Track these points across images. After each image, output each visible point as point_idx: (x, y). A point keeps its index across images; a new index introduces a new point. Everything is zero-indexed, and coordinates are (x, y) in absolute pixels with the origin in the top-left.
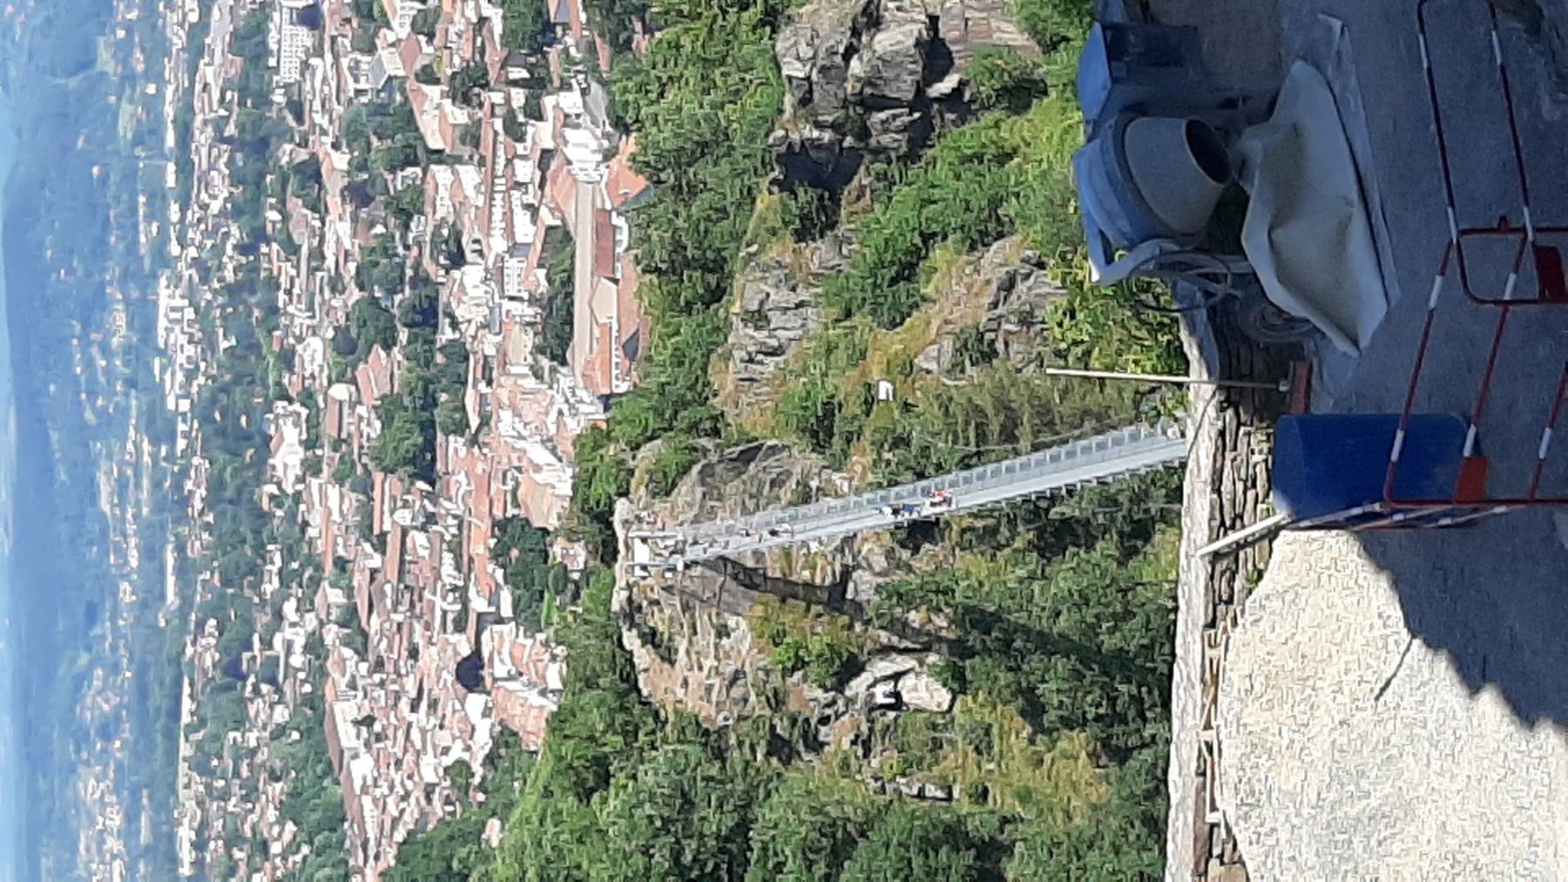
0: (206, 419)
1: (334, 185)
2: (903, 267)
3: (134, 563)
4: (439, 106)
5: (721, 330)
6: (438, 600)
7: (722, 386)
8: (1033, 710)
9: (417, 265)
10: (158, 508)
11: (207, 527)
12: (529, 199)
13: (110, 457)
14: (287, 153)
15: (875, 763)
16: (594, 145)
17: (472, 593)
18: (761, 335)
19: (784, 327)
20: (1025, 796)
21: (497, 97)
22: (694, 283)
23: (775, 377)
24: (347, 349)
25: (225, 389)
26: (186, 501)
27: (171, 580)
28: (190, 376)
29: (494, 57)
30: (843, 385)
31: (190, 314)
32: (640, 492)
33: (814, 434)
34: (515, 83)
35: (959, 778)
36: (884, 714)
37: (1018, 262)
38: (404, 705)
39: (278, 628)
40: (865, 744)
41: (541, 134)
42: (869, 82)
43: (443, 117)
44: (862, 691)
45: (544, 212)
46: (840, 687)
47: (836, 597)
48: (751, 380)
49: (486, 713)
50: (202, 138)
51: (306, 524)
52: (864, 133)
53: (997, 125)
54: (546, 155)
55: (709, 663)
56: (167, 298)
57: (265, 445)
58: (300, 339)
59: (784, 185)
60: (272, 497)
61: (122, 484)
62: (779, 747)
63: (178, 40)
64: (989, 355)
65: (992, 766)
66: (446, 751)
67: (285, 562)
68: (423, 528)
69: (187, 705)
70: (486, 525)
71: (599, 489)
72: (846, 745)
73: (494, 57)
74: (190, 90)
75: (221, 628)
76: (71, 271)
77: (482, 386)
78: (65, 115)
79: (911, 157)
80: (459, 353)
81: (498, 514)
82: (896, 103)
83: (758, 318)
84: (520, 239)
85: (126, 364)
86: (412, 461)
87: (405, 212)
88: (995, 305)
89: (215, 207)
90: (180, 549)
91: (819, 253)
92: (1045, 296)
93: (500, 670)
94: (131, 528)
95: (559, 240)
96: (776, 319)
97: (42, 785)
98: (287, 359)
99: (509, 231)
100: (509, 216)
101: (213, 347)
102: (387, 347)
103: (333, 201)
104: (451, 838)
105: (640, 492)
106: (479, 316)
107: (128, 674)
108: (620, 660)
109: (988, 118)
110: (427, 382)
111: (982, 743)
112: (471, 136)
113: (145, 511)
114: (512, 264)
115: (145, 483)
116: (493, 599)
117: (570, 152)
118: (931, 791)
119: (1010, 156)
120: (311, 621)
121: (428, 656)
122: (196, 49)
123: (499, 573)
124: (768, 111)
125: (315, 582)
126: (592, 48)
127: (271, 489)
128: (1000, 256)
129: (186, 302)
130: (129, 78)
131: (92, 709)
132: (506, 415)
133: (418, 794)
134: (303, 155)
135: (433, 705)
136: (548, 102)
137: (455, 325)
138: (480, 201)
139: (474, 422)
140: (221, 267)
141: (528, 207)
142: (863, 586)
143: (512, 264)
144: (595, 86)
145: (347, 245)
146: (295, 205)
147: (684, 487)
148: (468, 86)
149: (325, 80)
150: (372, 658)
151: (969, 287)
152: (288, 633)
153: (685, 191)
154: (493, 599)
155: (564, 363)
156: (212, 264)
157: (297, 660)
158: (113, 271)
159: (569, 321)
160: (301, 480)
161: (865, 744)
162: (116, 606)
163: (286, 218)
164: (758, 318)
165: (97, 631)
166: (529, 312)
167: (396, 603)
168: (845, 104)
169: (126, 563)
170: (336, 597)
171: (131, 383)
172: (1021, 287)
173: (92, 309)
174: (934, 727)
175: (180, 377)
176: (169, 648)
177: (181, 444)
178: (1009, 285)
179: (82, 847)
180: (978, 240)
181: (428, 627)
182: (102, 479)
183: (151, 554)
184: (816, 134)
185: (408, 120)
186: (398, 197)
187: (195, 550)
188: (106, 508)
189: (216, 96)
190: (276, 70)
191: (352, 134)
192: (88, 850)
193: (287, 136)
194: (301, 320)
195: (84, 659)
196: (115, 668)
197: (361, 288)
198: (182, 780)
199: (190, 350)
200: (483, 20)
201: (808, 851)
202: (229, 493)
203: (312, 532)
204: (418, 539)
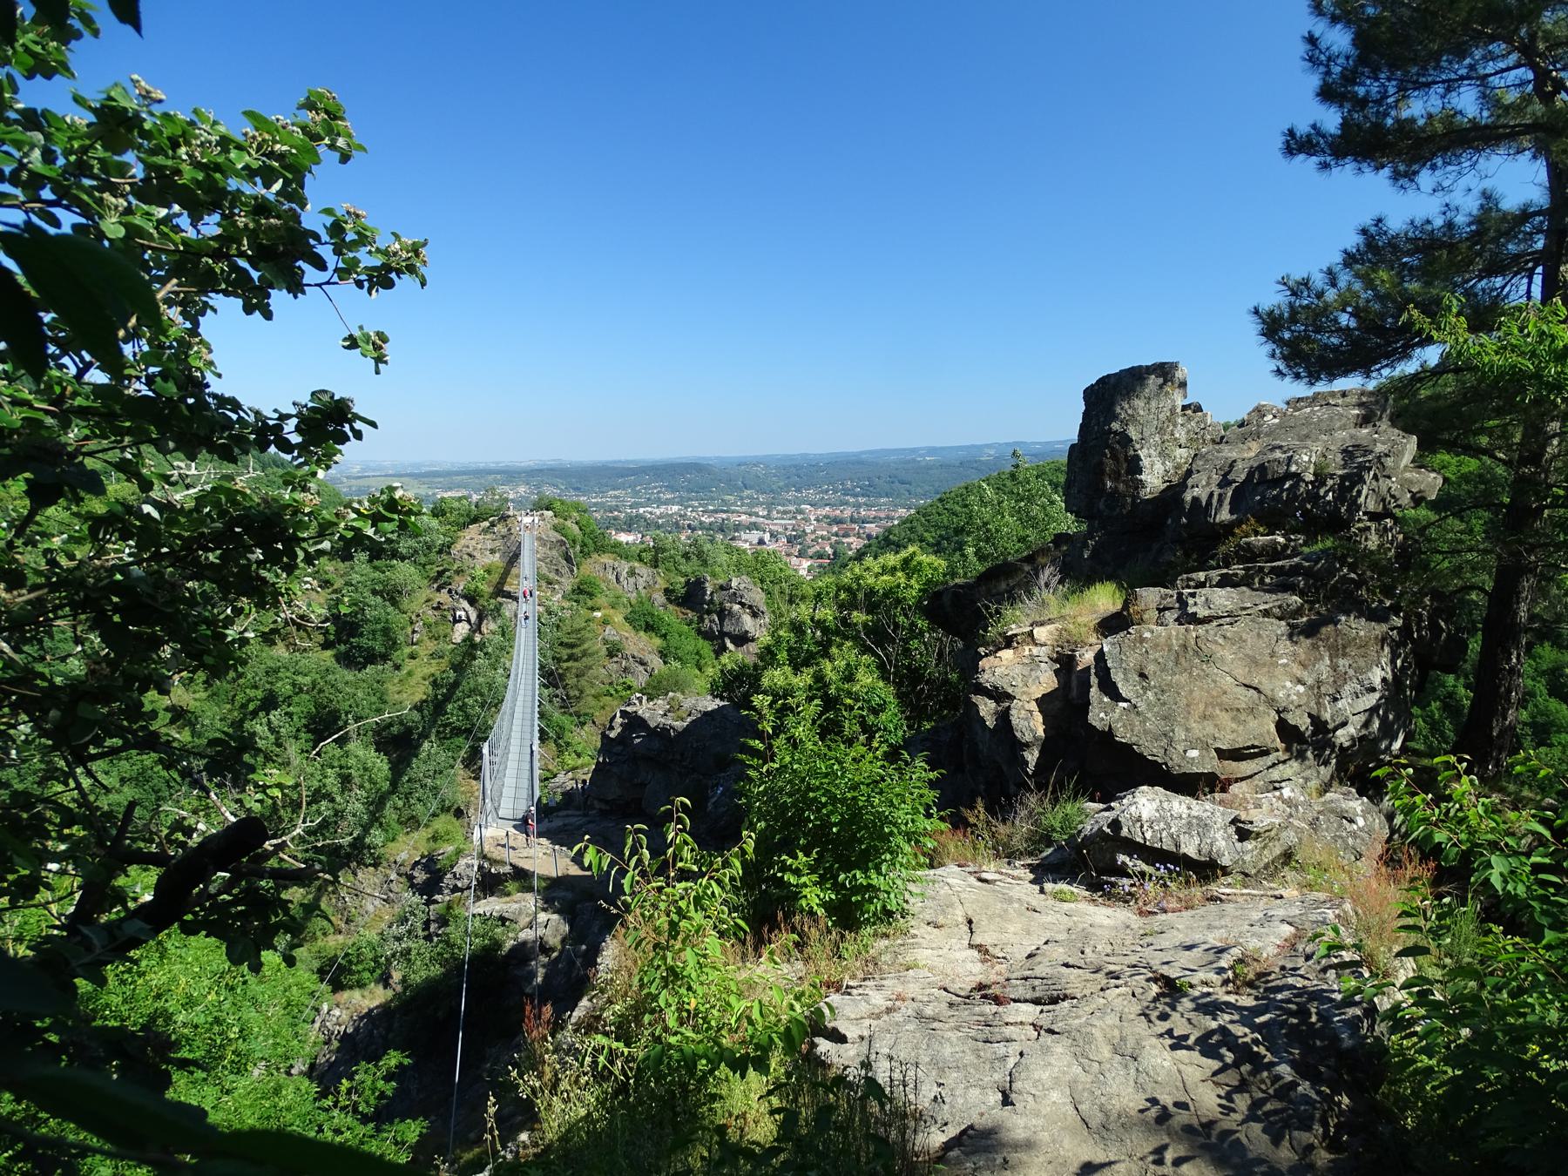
18: (624, 574)
28: (651, 513)
30: (601, 600)
32: (556, 521)
42: (730, 612)
46: (465, 597)
50: (724, 516)
52: (709, 612)
56: (675, 508)
79: (699, 632)
88: (633, 657)
91: (660, 598)
96: (632, 580)
105: (556, 521)
118: (416, 637)
119: (700, 670)
128: (656, 662)
130: (742, 499)
147: (556, 534)
158: (684, 494)
164: (632, 573)
168: (721, 604)
172: (641, 668)
174: (445, 637)
178: (642, 663)
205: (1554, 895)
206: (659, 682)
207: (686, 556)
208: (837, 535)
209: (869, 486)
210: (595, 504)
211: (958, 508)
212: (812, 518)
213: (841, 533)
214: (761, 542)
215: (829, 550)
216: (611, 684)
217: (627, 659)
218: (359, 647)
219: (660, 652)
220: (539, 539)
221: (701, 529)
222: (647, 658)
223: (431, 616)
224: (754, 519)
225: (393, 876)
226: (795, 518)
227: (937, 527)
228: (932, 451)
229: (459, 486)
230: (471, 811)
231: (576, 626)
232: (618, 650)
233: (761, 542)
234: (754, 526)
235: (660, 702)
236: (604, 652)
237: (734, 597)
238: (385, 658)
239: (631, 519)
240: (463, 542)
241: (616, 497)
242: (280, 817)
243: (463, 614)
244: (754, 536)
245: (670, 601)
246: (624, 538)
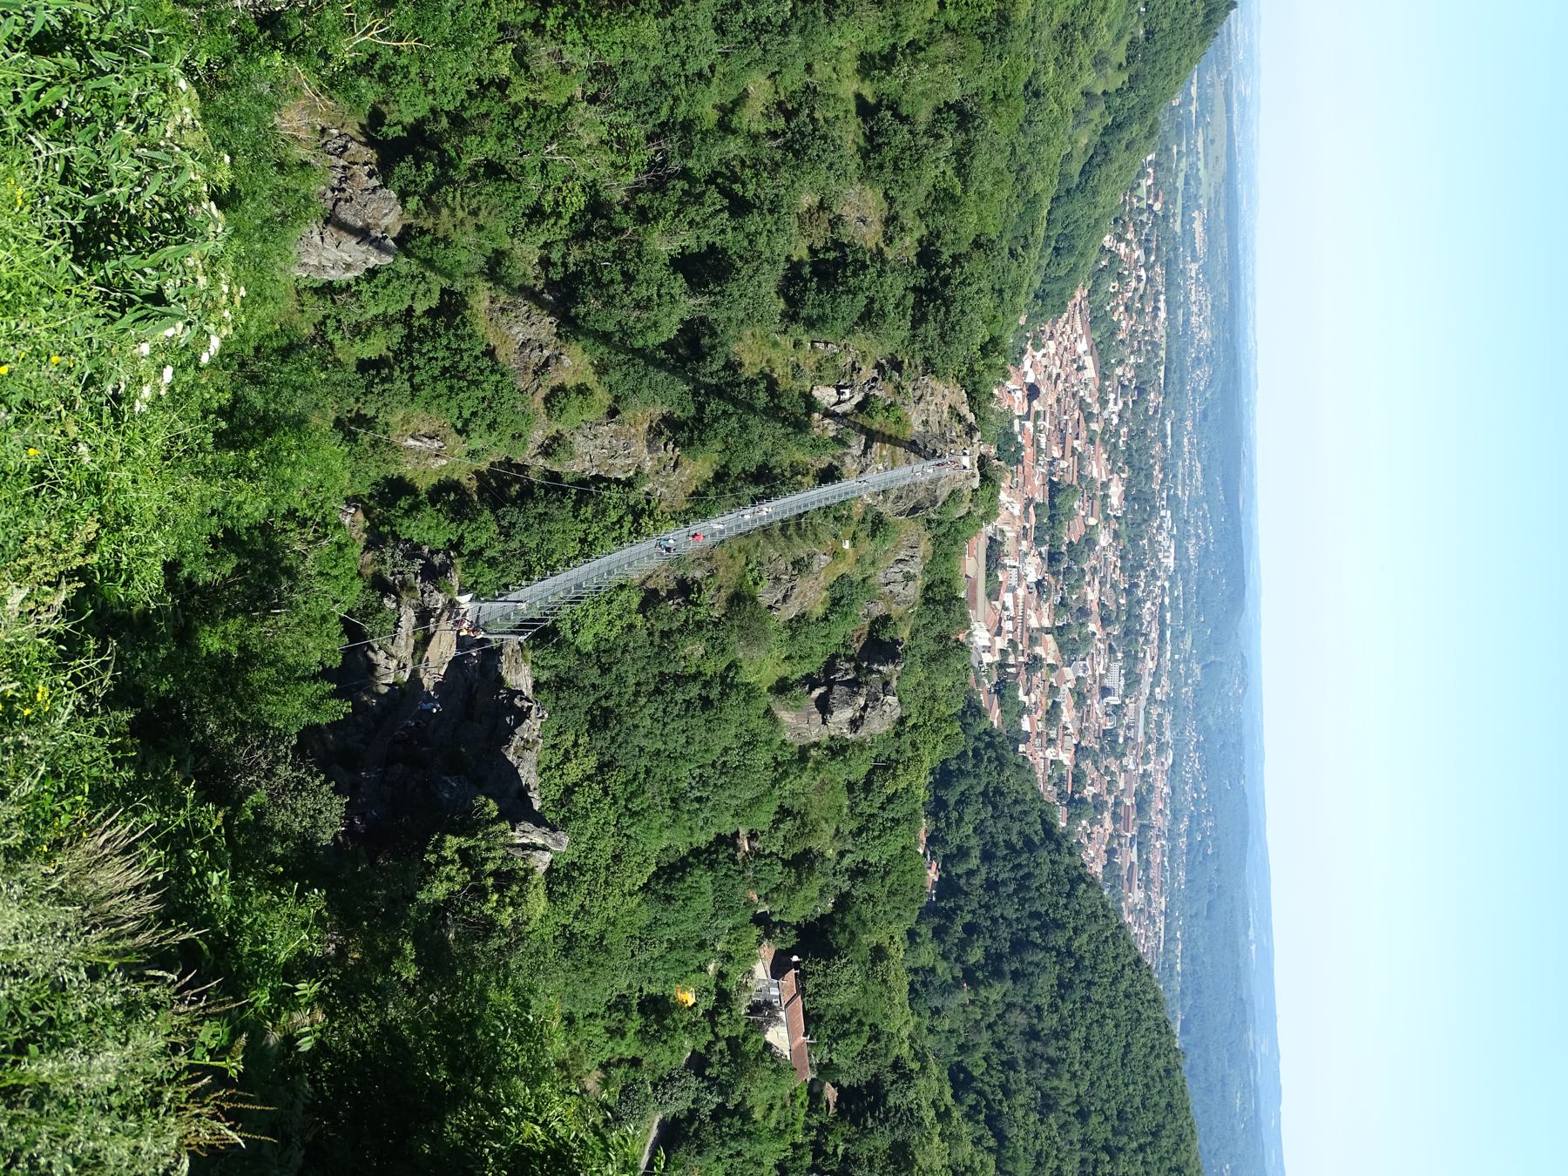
0: (1153, 507)
1: (1095, 616)
2: (838, 604)
3: (1186, 440)
4: (1048, 654)
5: (927, 571)
6: (1047, 426)
8: (772, 384)
9: (1057, 581)
10: (1174, 465)
11: (1153, 457)
12: (1006, 613)
13: (1197, 488)
14: (1116, 630)
15: (849, 359)
16: (977, 639)
17: (1032, 430)
19: (896, 573)
20: (775, 344)
21: (1021, 659)
22: (940, 593)
24: (1089, 541)
25: (1145, 521)
26: (1162, 469)
27: (1169, 432)
28: (1160, 527)
29: (1023, 677)
30: (867, 547)
31: (1160, 555)
33: (881, 522)
34: (1013, 666)
38: (1063, 377)
39: (1120, 411)
40: (854, 368)
41: (1001, 643)
42: (856, 694)
43: (1046, 649)
45: (999, 607)
46: (867, 398)
47: (872, 436)
49: (1025, 374)
50: (1154, 635)
51: (1108, 460)
52: (857, 668)
53: (793, 673)
54: (999, 633)
55: (932, 407)
56: (1170, 562)
57: (1126, 496)
58: (1110, 545)
59: (897, 642)
60: (1123, 472)
61: (1191, 475)
62: (897, 366)
63: (1164, 680)
64: (796, 563)
66: (1044, 356)
67: (1117, 442)
68: (1054, 459)
69: (1162, 375)
70: (1026, 461)
71: (986, 493)
72: (864, 368)
73: (1023, 677)
74: (1160, 656)
75: (1147, 410)
76: (1214, 573)
77: (1028, 526)
78: (1216, 644)
79: (835, 657)
80: (1038, 541)
81: (1020, 467)
82: (842, 683)
83: (908, 577)
84: (1011, 595)
86: (1059, 490)
87: (1063, 603)
88: (792, 588)
89: (1148, 604)
90: (1165, 446)
91: (878, 609)
93: (1019, 394)
94: (1187, 456)
95: (993, 594)
96: (899, 577)
97: (1228, 336)
98: (1116, 536)
99: (1015, 598)
100: (1016, 606)
101: (1150, 539)
102: (1071, 542)
103: (1095, 608)
104: (1042, 315)
105: (967, 493)
106: (1029, 559)
108: (976, 407)
109: (797, 676)
110: (1053, 527)
112: (1033, 641)
114: (1014, 582)
115: (1180, 476)
116: (1022, 427)
117: (988, 635)
118: (821, 346)
120: (1106, 414)
121: (1051, 400)
122: (1156, 675)
123: (1020, 439)
124: (905, 677)
125: (1104, 433)
126: (978, 682)
127: (1123, 476)
128: (791, 611)
132: (1017, 512)
133: (1057, 335)
134: (1109, 629)
135: (1050, 377)
136: (997, 658)
137: (1040, 554)
138: (1029, 612)
139: (1031, 509)
140: (1146, 577)
141: (1007, 609)
142: (857, 444)
143: (1014, 582)
144: (976, 665)
145: (1089, 589)
146: (1113, 607)
147: (946, 494)
148: (1035, 663)
149: (1099, 664)
150: (1078, 399)
151: (805, 596)
152: (1116, 409)
153: (942, 638)
154: (1022, 427)
155: (990, 538)
156: (1150, 578)
157: (1112, 396)
159: (988, 557)
160: (1110, 480)
161: (854, 368)
163: (1117, 601)
164: (908, 577)
166: (1007, 561)
167: (1066, 424)
168: (867, 683)
170: (1094, 426)
171: (1187, 522)
172: (780, 596)
173: (1204, 554)
175: (1165, 525)
176: (1169, 400)
177: (1164, 495)
178: (785, 598)
180: (801, 618)
181: (1052, 413)
183: (1178, 444)
184: (881, 668)
185: (1061, 647)
186: (1066, 612)
187: (1158, 447)
188: (1198, 465)
189: (1148, 656)
190: (1120, 668)
191: (1088, 639)
193: (1117, 638)
194: (1110, 555)
196: (1194, 390)
197: (1083, 570)
198: (1164, 339)
199: (1160, 538)
200: (1027, 694)
201: (882, 315)
202: (1143, 474)
203: (1105, 456)
204: (1056, 453)
206: (757, 620)
208: (1117, 804)
209: (1205, 855)
211: (1124, 985)
212: (1150, 767)
213: (1121, 811)
214: (1105, 691)
215: (1089, 792)
216: (760, 564)
217: (790, 580)
218: (805, 290)
219: (804, 615)
221: (1129, 602)
223: (845, 361)
224: (1147, 680)
225: (546, 353)
226: (1149, 741)
227: (1096, 953)
228: (1267, 955)
229: (1211, 244)
230: (613, 426)
233: (1105, 691)
234: (1132, 680)
237: (873, 698)
242: (609, 239)
244: (1116, 681)
245: (873, 623)
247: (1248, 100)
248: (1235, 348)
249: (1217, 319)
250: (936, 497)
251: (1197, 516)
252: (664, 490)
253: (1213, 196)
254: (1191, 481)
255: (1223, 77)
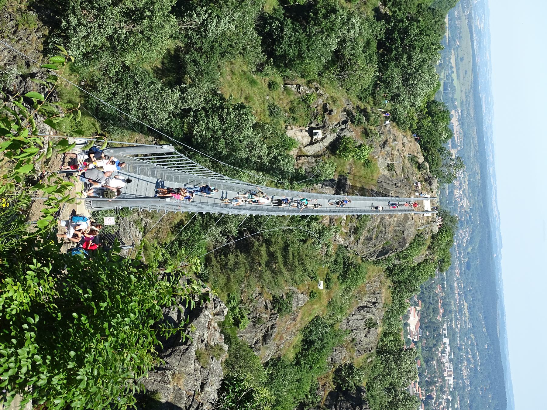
3: (456, 285)
7: (386, 290)
13: (465, 322)
15: (320, 101)
18: (369, 316)
23: (363, 295)
28: (443, 351)
30: (338, 289)
35: (281, 94)
36: (317, 125)
37: (262, 348)
44: (328, 136)
48: (374, 294)
56: (451, 380)
57: (421, 325)
60: (418, 305)
65: (267, 98)
72: (334, 109)
76: (482, 390)
85: (461, 356)
88: (272, 327)
92: (248, 332)
94: (457, 297)
96: (362, 324)
107: (455, 244)
111: (273, 110)
113: (453, 303)
127: (418, 308)
129: (446, 378)
131: (466, 231)
147: (412, 236)
151: (281, 338)
162: (460, 269)
165: (466, 260)
169: (458, 284)
171: (460, 349)
172: (260, 336)
173: (474, 374)
174: (294, 119)
178: (266, 337)
179: (467, 182)
182: (467, 314)
188: (465, 304)
192: (465, 182)
195: (469, 249)
199: (444, 360)
205: (52, 263)
207: (391, 388)
210: (452, 288)
217: (270, 319)
220: (406, 218)
222: (272, 344)
223: (316, 103)
229: (466, 135)
231: (307, 263)
232: (280, 310)
235: (218, 334)
236: (279, 293)
238: (269, 52)
239: (436, 329)
240: (400, 134)
241: (461, 311)
243: (320, 136)
246: (413, 320)
247: (482, 32)
248: (487, 214)
249: (473, 192)
250: (404, 238)
251: (466, 345)
252: (149, 220)
253: (465, 100)
254: (461, 316)
255: (467, 13)
